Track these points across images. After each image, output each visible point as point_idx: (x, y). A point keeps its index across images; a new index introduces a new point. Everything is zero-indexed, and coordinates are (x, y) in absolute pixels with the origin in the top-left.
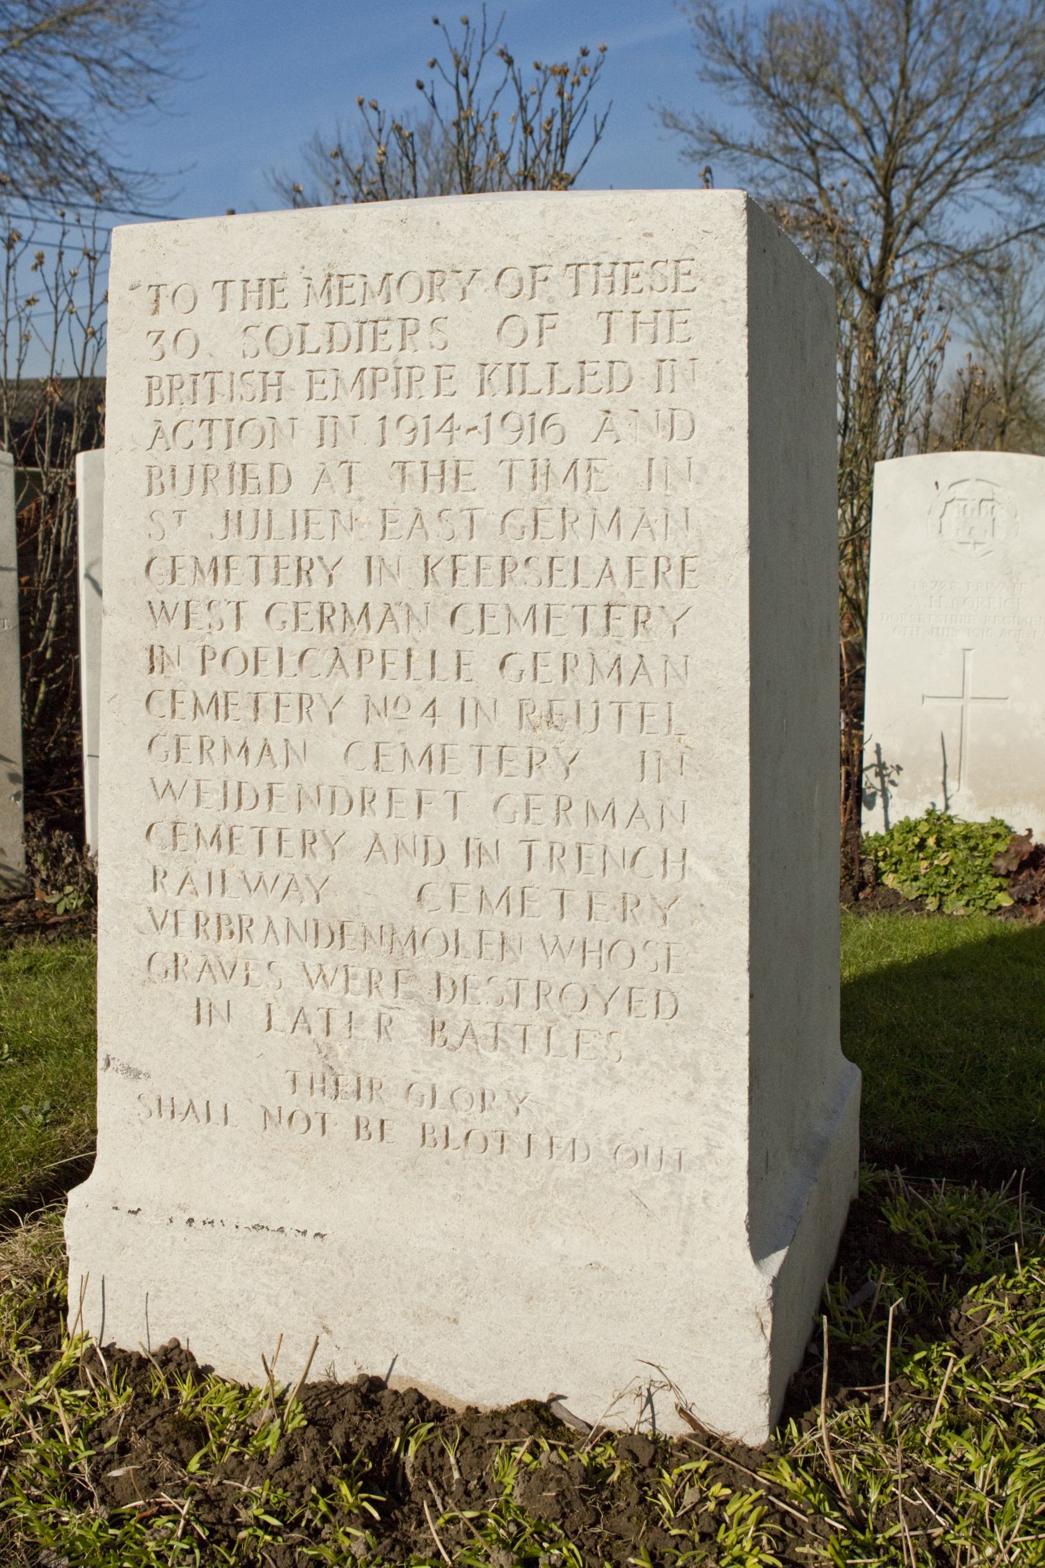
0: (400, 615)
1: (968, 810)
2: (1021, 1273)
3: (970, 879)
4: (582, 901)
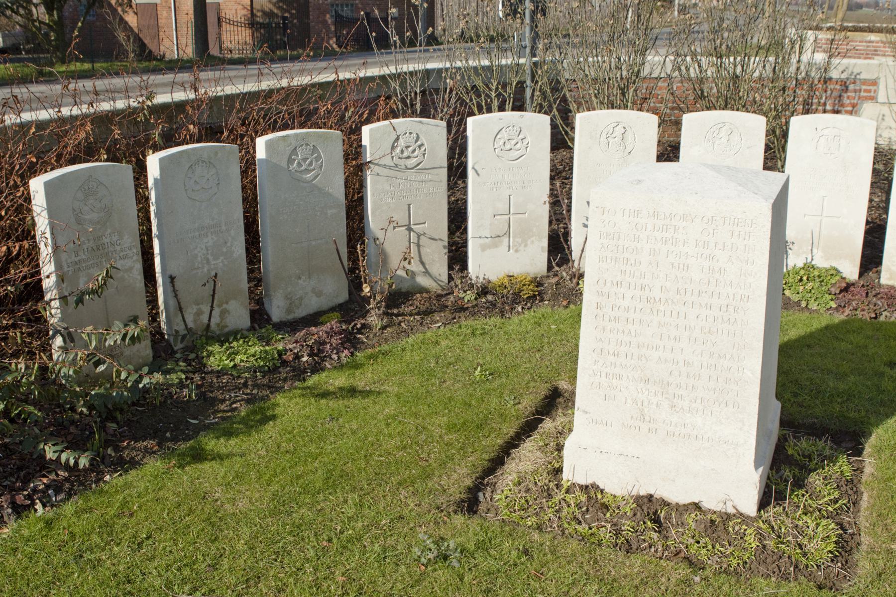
0: (670, 302)
1: (821, 262)
2: (827, 468)
3: (819, 296)
4: (715, 378)
